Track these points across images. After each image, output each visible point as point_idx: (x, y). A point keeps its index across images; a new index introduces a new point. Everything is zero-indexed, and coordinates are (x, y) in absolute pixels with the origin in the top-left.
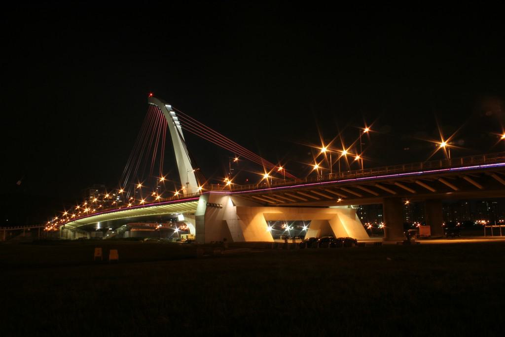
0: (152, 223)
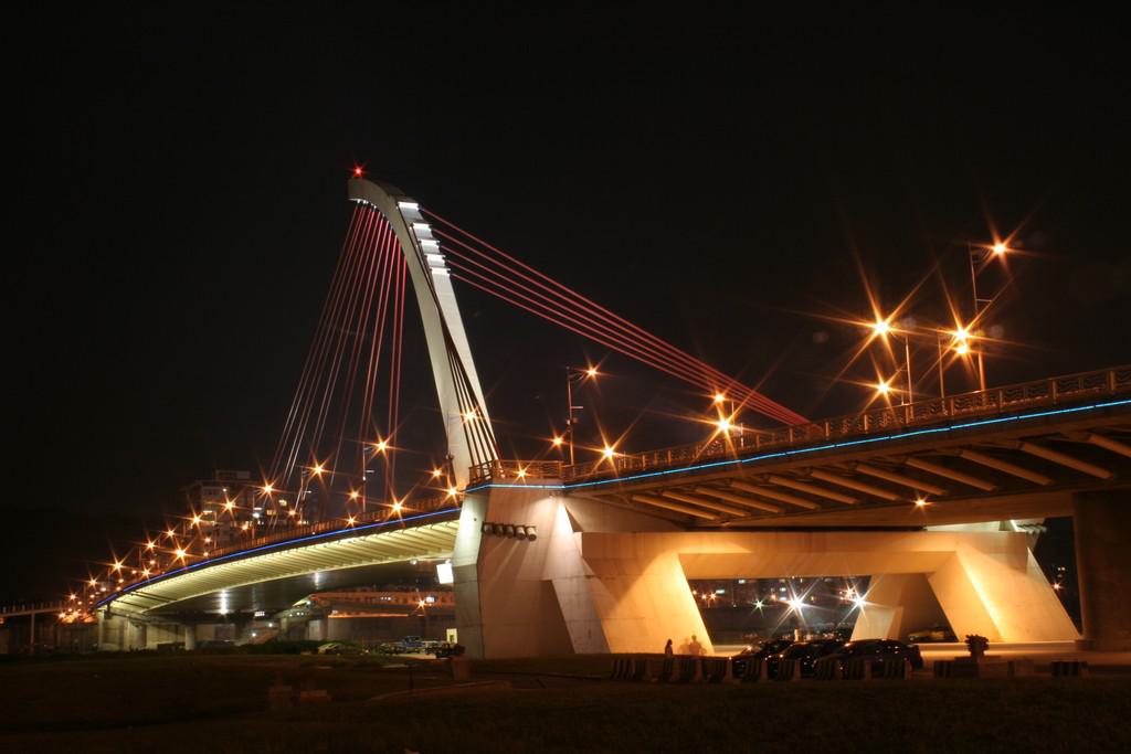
0: (402, 590)
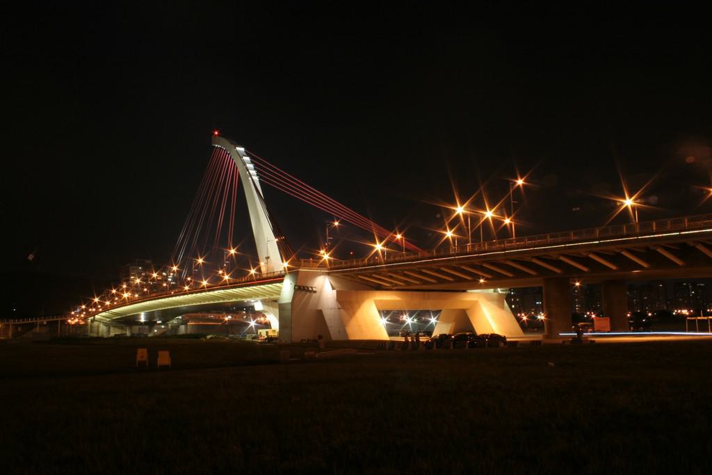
0: (217, 313)
